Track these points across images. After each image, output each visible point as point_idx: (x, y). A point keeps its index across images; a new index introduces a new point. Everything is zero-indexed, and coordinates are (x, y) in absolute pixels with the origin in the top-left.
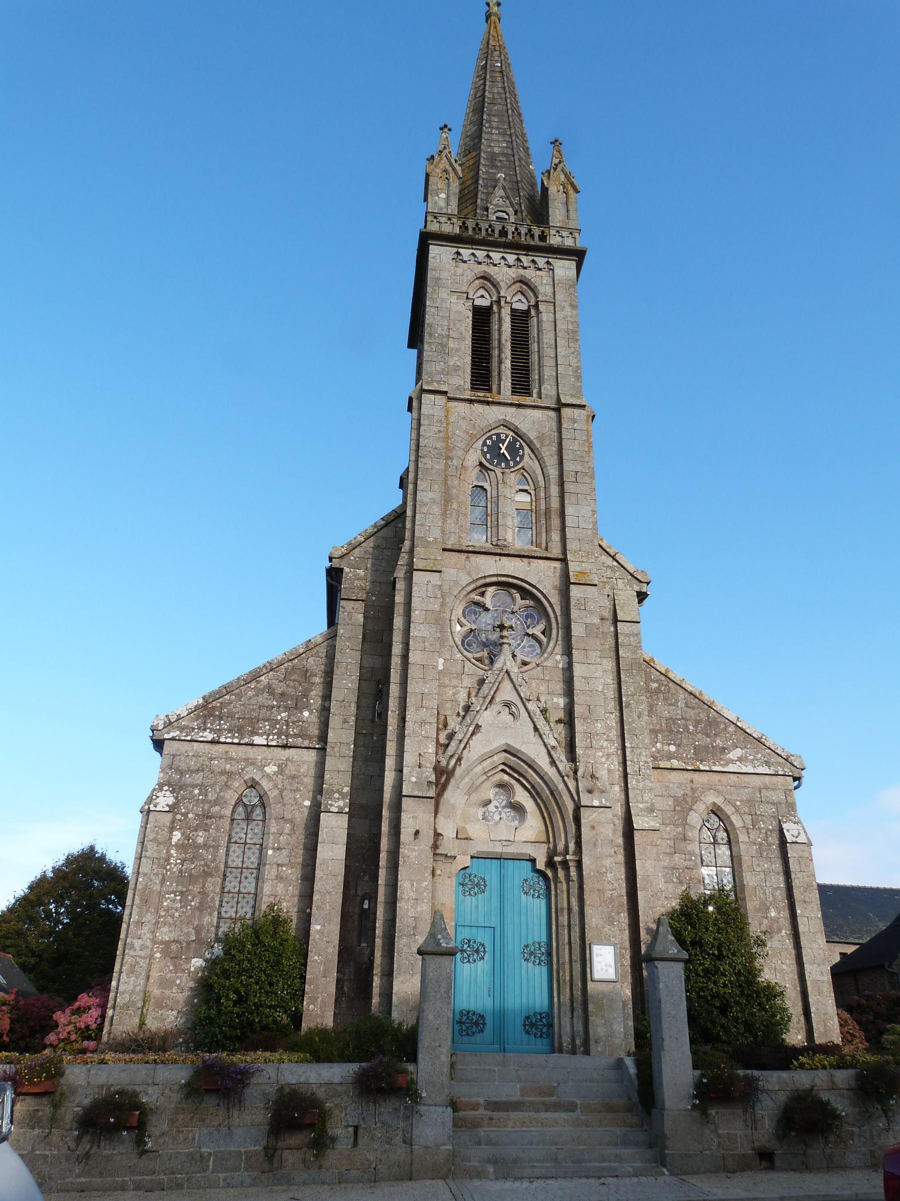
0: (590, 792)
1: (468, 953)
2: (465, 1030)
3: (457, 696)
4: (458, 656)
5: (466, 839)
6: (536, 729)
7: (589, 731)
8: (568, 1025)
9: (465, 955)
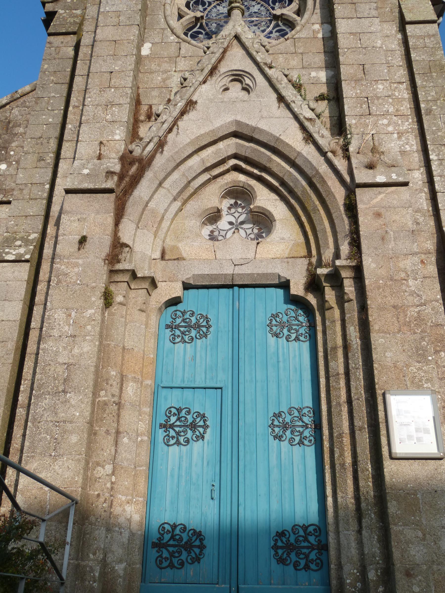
0: (371, 166)
1: (177, 429)
2: (166, 559)
3: (168, 82)
4: (172, 38)
5: (178, 259)
6: (281, 99)
7: (364, 95)
8: (353, 544)
9: (172, 433)
